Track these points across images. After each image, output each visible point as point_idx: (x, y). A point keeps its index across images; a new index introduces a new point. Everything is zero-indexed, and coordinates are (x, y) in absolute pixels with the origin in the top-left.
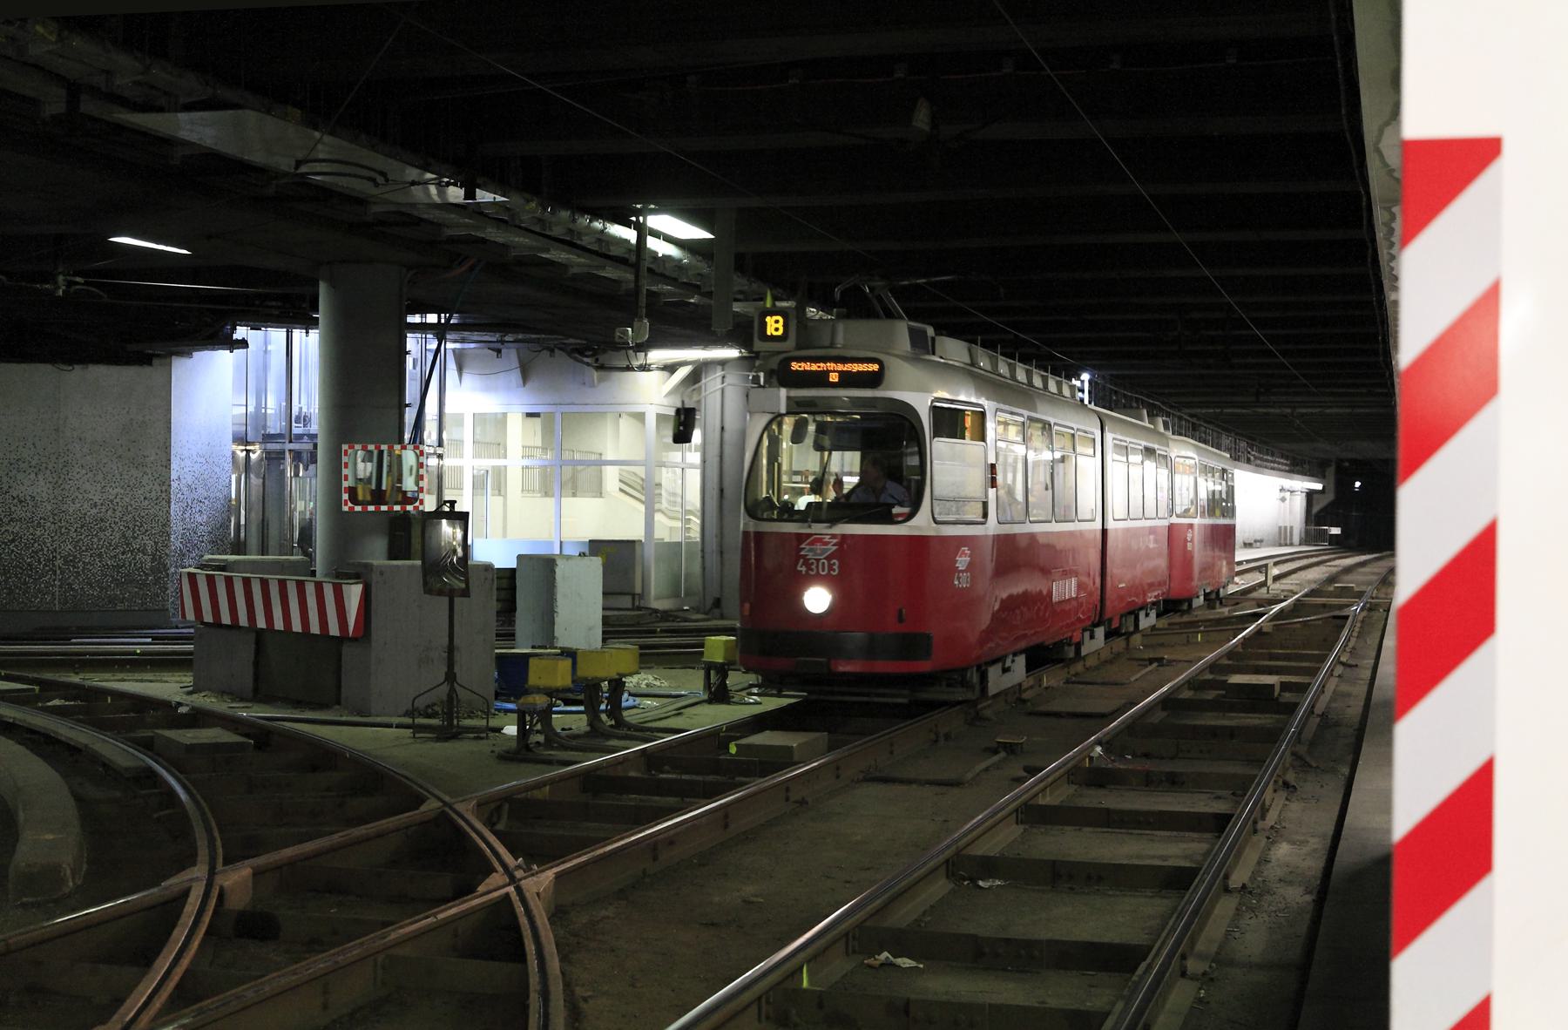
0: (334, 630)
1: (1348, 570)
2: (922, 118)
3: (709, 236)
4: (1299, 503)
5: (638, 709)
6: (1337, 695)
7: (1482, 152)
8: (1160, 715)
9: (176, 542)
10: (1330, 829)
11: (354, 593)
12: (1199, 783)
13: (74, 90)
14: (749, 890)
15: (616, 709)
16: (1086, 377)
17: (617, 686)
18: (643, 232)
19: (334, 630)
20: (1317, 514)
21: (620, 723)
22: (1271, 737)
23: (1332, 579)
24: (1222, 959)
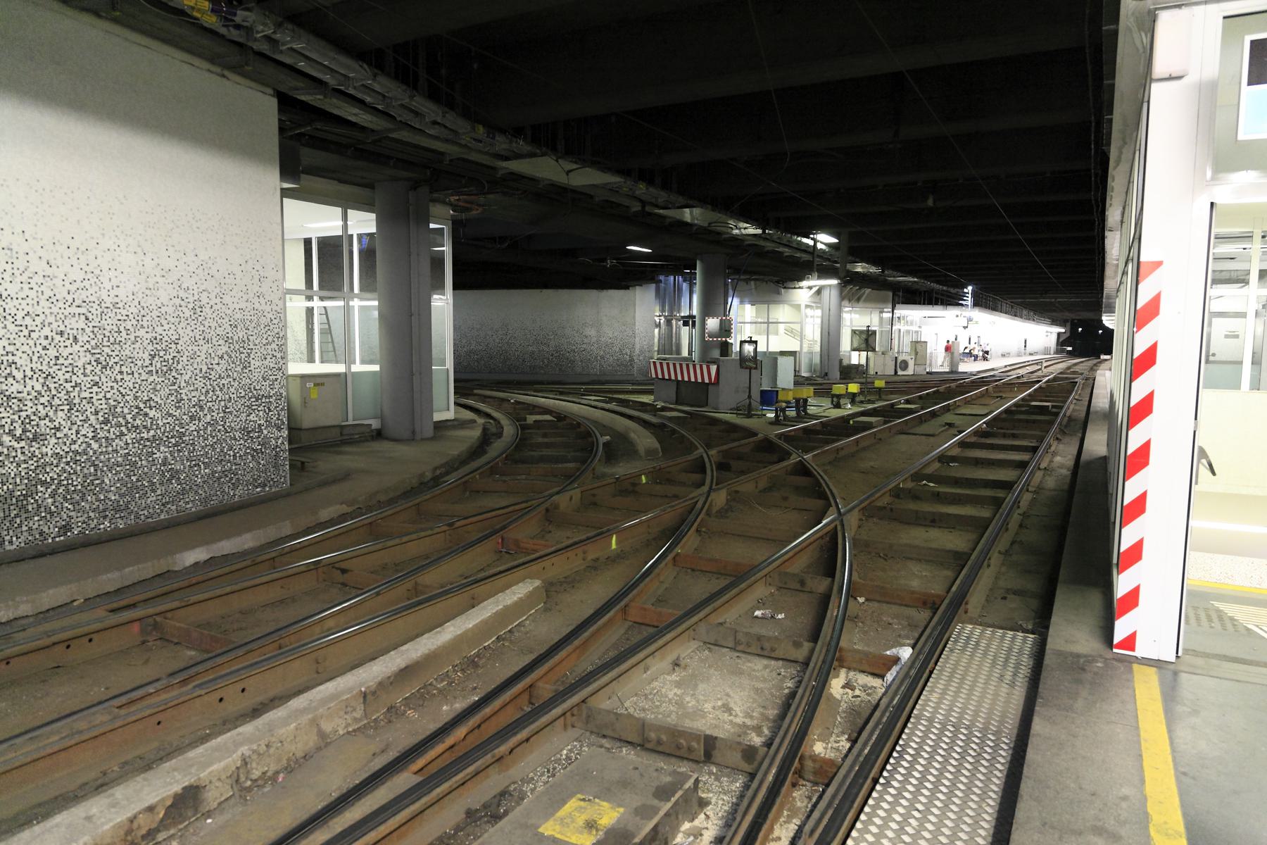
0: (707, 381)
1: (1076, 364)
2: (930, 202)
3: (836, 241)
4: (1054, 338)
5: (812, 410)
6: (1074, 410)
7: (1159, 264)
8: (1004, 416)
9: (637, 352)
10: (1075, 452)
11: (714, 368)
12: (1024, 437)
13: (644, 203)
14: (872, 463)
15: (805, 410)
16: (970, 288)
17: (806, 401)
18: (815, 241)
19: (707, 381)
20: (1061, 342)
21: (806, 413)
22: (1052, 423)
23: (1069, 368)
24: (1039, 489)
